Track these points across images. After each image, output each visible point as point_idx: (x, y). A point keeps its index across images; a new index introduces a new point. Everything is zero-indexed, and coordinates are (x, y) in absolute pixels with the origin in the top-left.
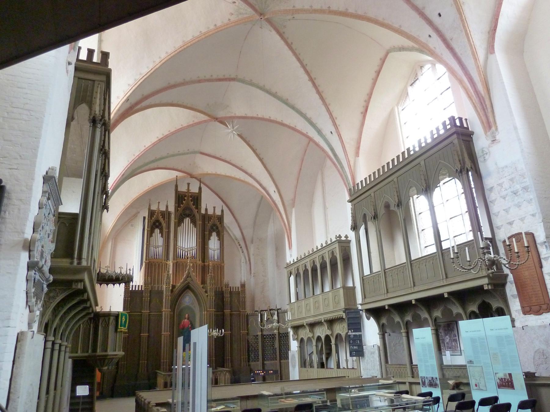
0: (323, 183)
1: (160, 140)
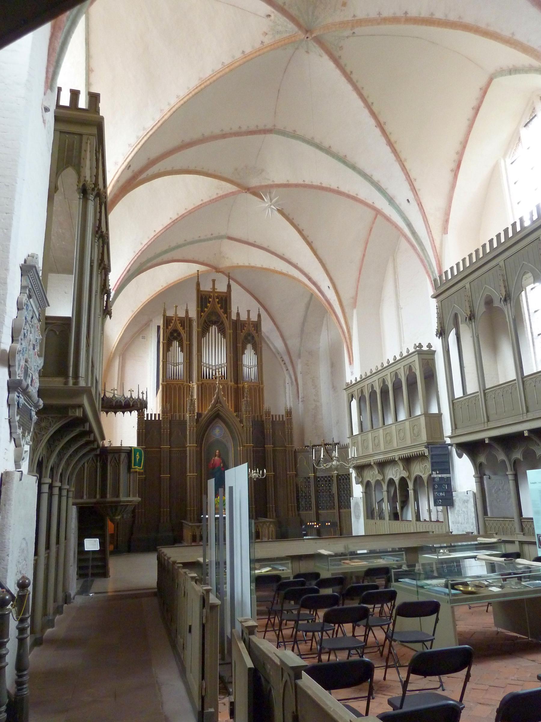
0: (395, 273)
1: (174, 223)
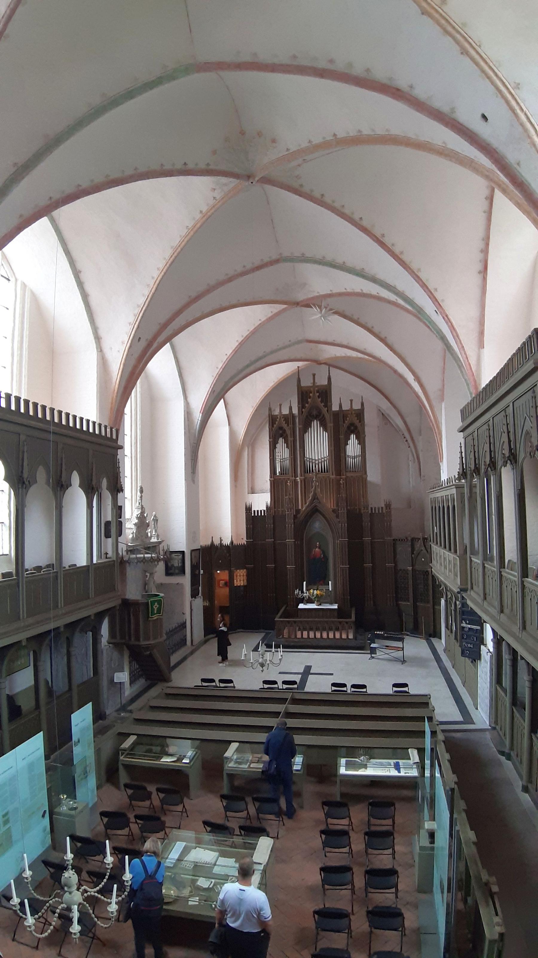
1: (241, 344)
